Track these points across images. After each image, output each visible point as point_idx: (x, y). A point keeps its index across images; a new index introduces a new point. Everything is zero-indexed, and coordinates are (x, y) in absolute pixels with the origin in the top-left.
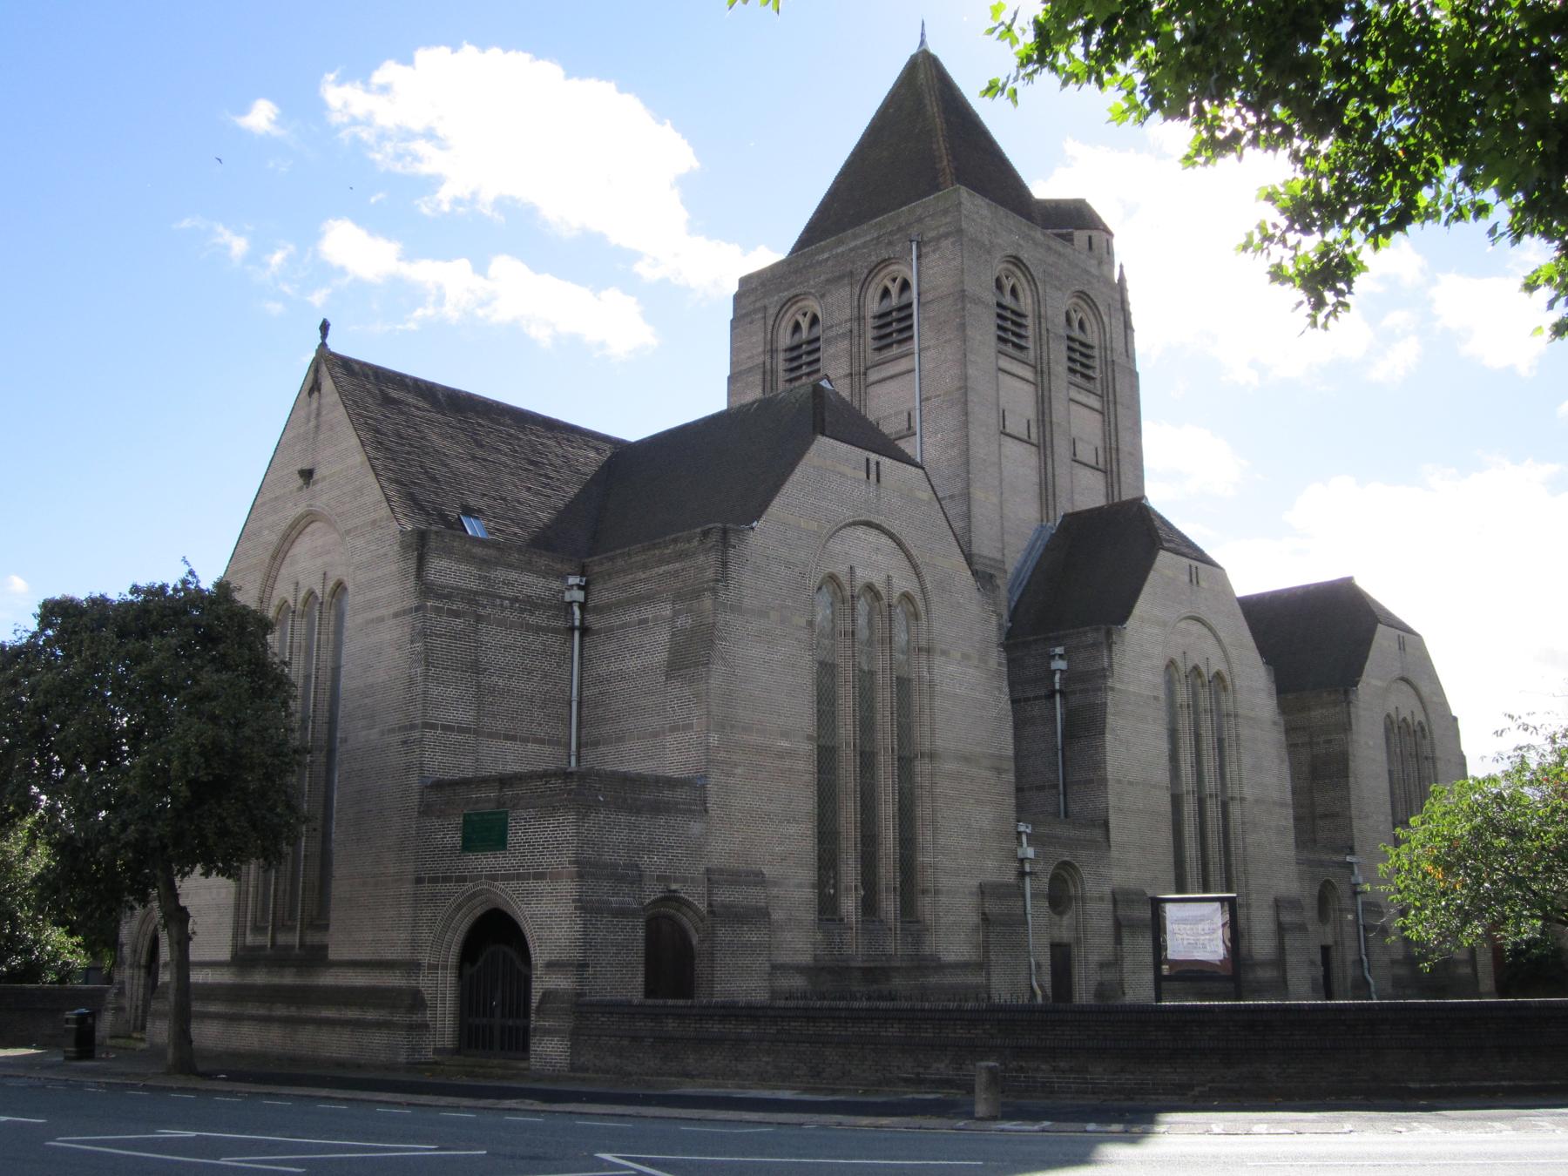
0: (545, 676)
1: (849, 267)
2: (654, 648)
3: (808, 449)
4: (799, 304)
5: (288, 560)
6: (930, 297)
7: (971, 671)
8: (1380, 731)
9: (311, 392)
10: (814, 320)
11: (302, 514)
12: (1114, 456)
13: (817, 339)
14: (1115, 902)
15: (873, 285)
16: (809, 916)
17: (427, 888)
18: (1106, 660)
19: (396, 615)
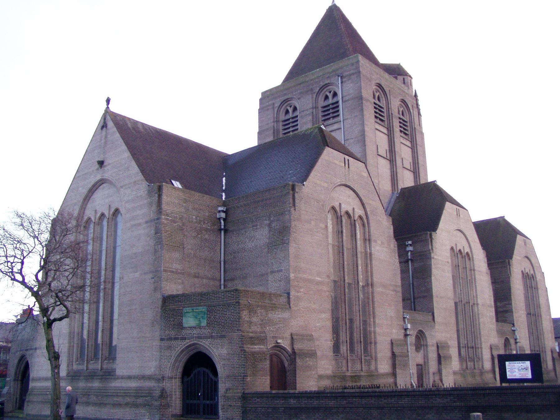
1: (311, 87)
3: (322, 152)
4: (288, 102)
6: (347, 98)
8: (520, 276)
9: (103, 127)
10: (295, 109)
12: (417, 166)
13: (297, 116)
14: (438, 347)
15: (321, 94)
16: (331, 353)
18: (430, 246)
19: (147, 222)
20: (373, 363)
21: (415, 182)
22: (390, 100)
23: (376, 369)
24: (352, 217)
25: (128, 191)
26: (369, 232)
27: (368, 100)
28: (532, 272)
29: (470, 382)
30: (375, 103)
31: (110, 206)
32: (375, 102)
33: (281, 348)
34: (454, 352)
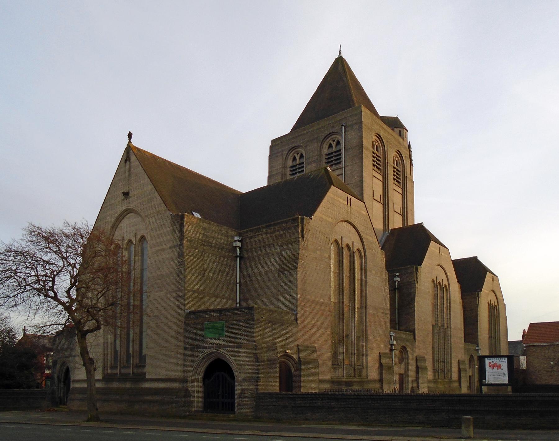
0: (227, 274)
2: (273, 264)
4: (296, 150)
5: (118, 229)
7: (377, 278)
10: (302, 156)
11: (124, 210)
13: (303, 163)
14: (417, 360)
16: (329, 363)
17: (189, 351)
19: (170, 248)
20: (364, 371)
21: (403, 224)
22: (387, 150)
23: (367, 377)
24: (352, 249)
25: (152, 220)
26: (365, 263)
27: (367, 149)
28: (496, 304)
29: (441, 388)
30: (373, 153)
31: (136, 233)
32: (374, 151)
33: (289, 357)
34: (429, 364)
